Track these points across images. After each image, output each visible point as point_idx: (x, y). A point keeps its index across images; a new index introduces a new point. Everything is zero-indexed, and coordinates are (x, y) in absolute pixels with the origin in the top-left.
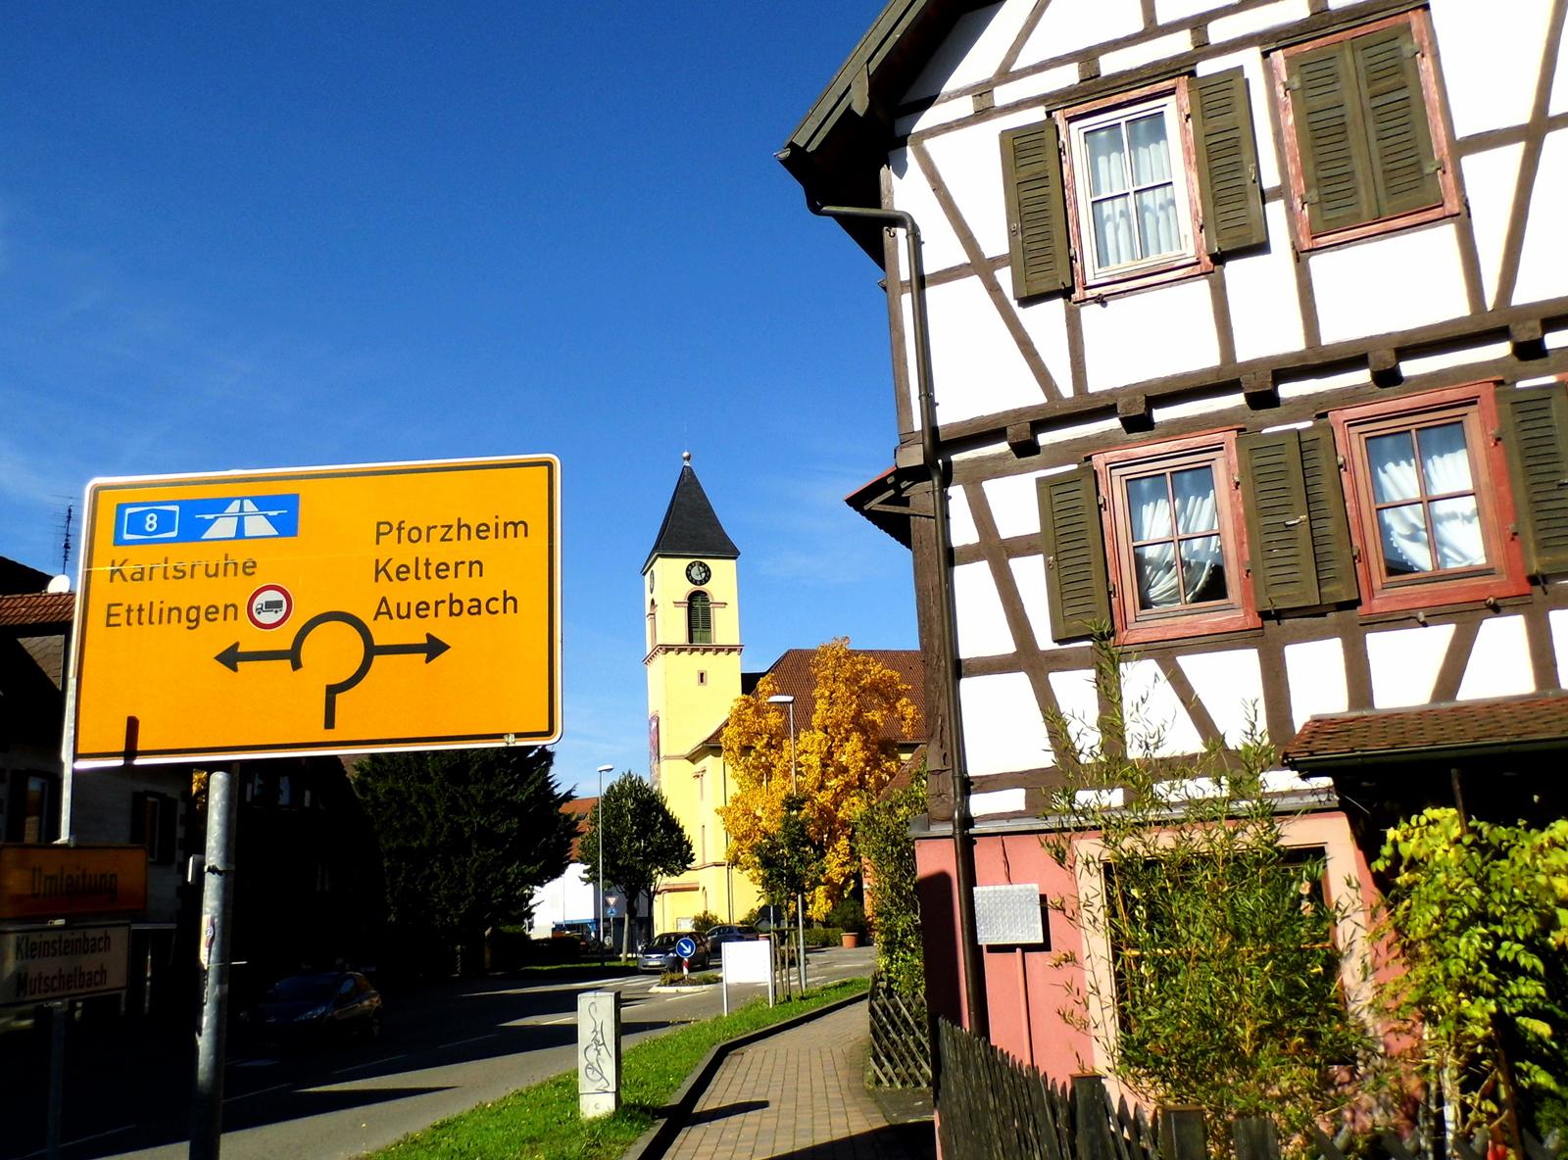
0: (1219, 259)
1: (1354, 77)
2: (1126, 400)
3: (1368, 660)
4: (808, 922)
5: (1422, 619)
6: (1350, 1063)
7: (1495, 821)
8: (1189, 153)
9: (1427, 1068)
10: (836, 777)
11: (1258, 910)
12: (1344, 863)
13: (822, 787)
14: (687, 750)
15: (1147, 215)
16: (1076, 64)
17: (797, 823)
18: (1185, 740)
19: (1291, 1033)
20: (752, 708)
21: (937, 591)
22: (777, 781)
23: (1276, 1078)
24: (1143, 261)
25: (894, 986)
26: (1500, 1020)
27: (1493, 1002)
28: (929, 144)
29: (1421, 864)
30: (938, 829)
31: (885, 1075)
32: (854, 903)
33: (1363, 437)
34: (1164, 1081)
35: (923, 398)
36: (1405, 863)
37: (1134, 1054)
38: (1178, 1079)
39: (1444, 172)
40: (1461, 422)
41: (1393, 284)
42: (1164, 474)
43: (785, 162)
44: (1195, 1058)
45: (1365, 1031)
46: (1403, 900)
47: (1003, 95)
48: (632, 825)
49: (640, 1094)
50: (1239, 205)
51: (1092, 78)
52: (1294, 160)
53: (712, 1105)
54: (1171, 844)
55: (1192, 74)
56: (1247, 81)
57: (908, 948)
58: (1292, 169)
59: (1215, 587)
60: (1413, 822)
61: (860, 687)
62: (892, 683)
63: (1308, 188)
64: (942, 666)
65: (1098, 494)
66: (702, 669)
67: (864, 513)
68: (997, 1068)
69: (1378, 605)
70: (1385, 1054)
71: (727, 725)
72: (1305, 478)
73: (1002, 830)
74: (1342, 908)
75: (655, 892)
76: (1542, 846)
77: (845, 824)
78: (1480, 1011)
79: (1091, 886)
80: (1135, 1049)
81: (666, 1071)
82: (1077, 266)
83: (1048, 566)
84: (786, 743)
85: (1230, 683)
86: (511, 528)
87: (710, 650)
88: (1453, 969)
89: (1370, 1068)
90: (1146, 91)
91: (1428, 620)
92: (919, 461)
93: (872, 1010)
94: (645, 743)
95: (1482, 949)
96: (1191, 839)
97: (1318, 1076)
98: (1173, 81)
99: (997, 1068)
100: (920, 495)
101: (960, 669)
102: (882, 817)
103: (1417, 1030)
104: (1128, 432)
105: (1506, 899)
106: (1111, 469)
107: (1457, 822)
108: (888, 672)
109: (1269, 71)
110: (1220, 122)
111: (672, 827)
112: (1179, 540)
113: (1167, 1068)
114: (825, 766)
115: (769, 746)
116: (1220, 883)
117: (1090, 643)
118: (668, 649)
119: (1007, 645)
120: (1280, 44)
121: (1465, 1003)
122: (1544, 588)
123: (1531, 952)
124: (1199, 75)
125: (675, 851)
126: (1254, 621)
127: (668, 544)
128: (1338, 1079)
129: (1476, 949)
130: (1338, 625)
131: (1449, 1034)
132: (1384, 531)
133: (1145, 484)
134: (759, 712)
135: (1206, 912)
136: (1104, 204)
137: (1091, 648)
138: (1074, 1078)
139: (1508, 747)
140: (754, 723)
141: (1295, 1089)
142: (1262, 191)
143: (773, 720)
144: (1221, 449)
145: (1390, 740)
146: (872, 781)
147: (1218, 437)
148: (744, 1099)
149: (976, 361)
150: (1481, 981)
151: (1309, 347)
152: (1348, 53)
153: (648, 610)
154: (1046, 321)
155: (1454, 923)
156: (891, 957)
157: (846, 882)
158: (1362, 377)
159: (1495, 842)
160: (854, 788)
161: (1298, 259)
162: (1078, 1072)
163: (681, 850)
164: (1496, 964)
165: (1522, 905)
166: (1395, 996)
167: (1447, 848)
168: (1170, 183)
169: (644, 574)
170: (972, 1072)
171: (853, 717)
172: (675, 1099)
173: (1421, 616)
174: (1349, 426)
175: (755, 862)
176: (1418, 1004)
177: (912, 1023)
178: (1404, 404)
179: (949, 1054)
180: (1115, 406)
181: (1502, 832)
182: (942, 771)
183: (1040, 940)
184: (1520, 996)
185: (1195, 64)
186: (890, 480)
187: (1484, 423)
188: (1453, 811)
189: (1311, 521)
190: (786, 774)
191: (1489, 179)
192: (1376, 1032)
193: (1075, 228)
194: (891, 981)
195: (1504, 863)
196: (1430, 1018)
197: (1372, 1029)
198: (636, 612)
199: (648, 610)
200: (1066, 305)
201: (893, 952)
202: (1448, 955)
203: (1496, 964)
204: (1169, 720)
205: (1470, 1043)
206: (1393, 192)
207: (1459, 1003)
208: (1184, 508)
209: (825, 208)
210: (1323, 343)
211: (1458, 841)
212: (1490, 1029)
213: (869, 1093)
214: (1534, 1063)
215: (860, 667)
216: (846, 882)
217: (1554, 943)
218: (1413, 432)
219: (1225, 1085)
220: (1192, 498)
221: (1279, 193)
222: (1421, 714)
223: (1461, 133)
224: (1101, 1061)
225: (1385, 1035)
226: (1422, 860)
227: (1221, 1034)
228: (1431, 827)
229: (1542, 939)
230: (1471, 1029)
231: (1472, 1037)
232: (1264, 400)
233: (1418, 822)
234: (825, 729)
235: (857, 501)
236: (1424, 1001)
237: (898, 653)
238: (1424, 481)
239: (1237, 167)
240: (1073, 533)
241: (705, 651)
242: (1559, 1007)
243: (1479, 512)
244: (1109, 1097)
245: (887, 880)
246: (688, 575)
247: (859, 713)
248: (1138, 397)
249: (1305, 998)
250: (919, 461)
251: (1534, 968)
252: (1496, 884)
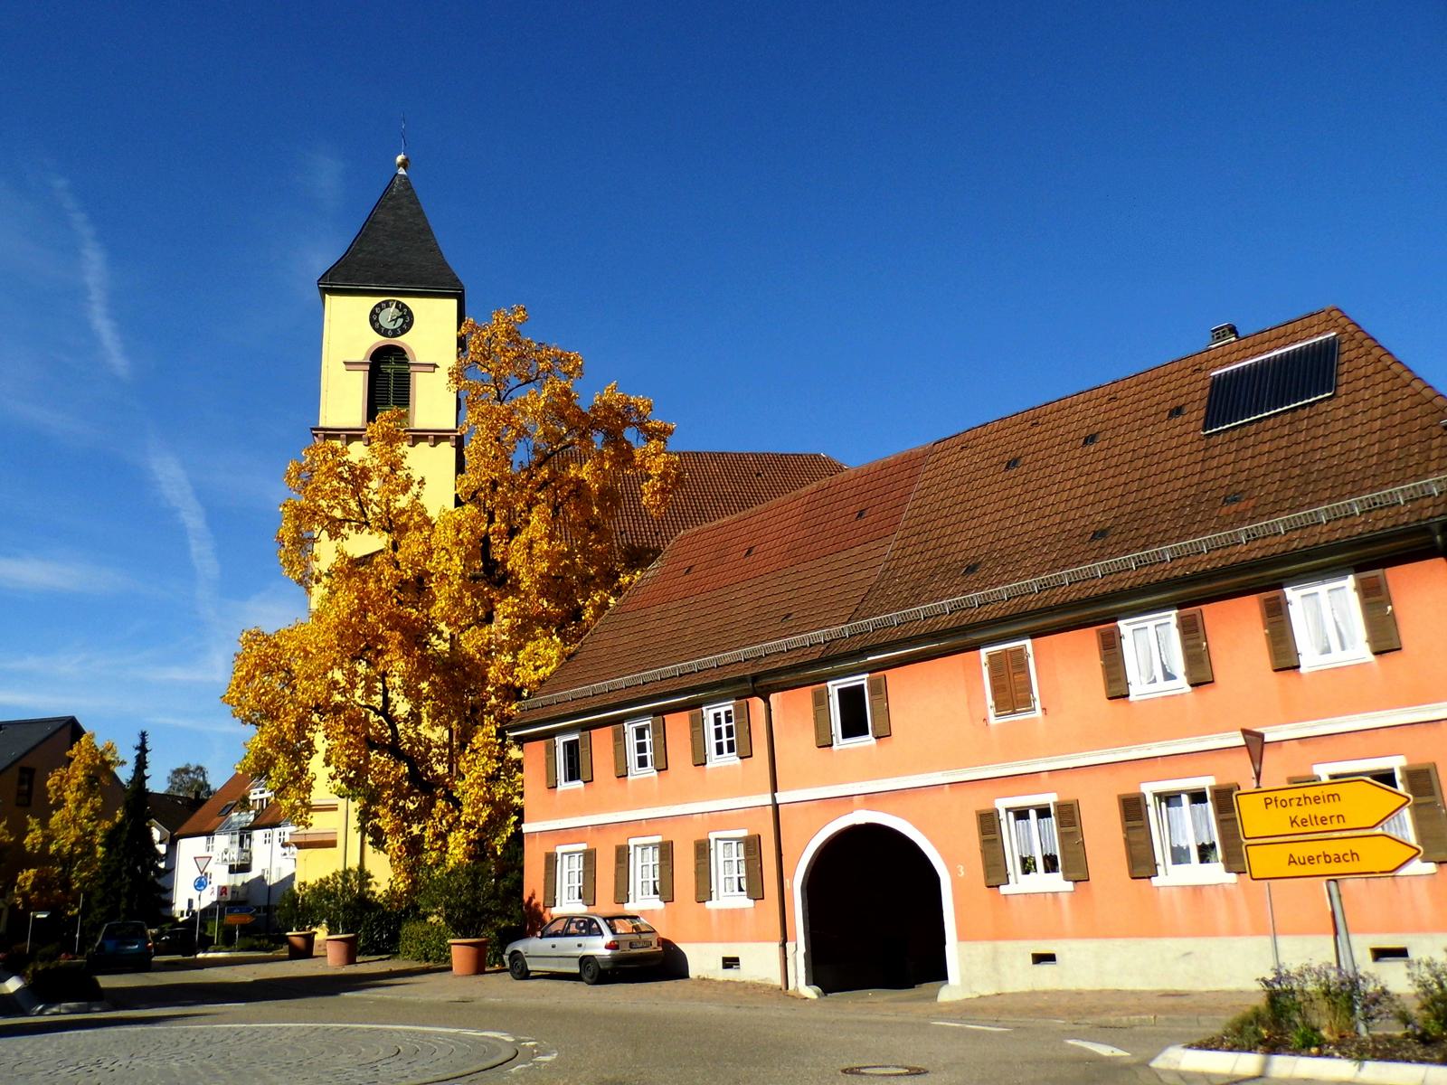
86: (1331, 797)
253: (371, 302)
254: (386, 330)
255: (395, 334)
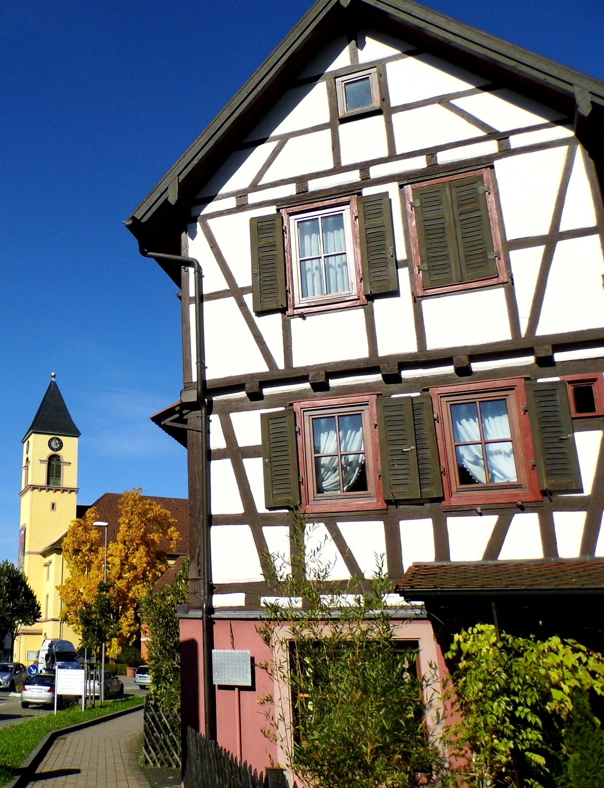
0: (371, 298)
1: (451, 204)
2: (314, 373)
3: (448, 533)
4: (107, 659)
5: (479, 511)
6: (427, 772)
7: (516, 635)
8: (356, 238)
9: (473, 779)
10: (129, 572)
11: (378, 677)
12: (429, 653)
13: (120, 577)
14: (41, 549)
15: (331, 270)
16: (294, 185)
17: (105, 600)
18: (340, 573)
19: (394, 752)
20: (82, 527)
21: (200, 474)
22: (94, 572)
23: (384, 778)
24: (328, 296)
25: (159, 704)
26: (516, 753)
27: (512, 742)
28: (210, 222)
29: (473, 656)
30: (192, 614)
31: (151, 758)
32: (134, 649)
33: (448, 403)
34: (320, 776)
35: (199, 364)
36: (464, 655)
37: (302, 758)
38: (327, 775)
39: (499, 259)
40: (505, 399)
41: (468, 319)
42: (334, 417)
43: (129, 227)
44: (339, 763)
45: (437, 754)
46: (462, 678)
47: (253, 198)
48: (6, 593)
49: (4, 759)
50: (382, 269)
51: (303, 192)
52: (415, 246)
53: (47, 769)
54: (329, 635)
55: (360, 194)
56: (390, 200)
57: (168, 680)
58: (414, 251)
59: (360, 484)
60: (470, 632)
61: (146, 519)
62: (166, 517)
63: (422, 262)
64: (199, 516)
65: (296, 425)
66: (54, 501)
67: (160, 426)
68: (222, 760)
69: (455, 501)
70: (449, 768)
71: (66, 535)
72: (414, 425)
73: (230, 617)
74: (427, 679)
75: (17, 634)
76: (544, 651)
77: (133, 601)
78: (504, 746)
79: (281, 655)
80: (304, 755)
81: (19, 746)
82: (290, 296)
83: (265, 465)
84: (100, 549)
85: (367, 540)
87: (59, 490)
88: (489, 720)
89: (439, 776)
90: (333, 202)
91: (482, 512)
92: (195, 399)
93: (145, 718)
94: (17, 541)
95: (506, 709)
96: (341, 633)
97: (409, 778)
98: (349, 197)
99: (222, 760)
100: (194, 418)
101: (211, 520)
102: (158, 601)
103: (467, 755)
104: (314, 392)
105: (521, 681)
106: (304, 411)
107: (495, 634)
108: (164, 511)
109: (403, 196)
110: (373, 222)
111: (30, 595)
112: (341, 455)
113: (322, 768)
114: (123, 564)
115: (90, 550)
116: (357, 661)
117: (287, 511)
118: (34, 488)
119: (238, 508)
120: (410, 181)
121: (496, 741)
122: (550, 498)
123: (535, 714)
124: (364, 195)
125: (30, 610)
126: (382, 505)
127: (39, 426)
128: (421, 781)
129: (503, 710)
130: (430, 510)
131: (486, 759)
132: (459, 458)
133: (323, 421)
134: (86, 529)
135: (348, 676)
136: (307, 262)
137: (288, 513)
138: (267, 770)
139: (525, 592)
140: (82, 536)
141: (395, 785)
142: (396, 261)
143: (94, 535)
144: (367, 404)
145: (458, 582)
146: (150, 575)
147: (366, 398)
148: (66, 767)
149: (229, 346)
150: (505, 729)
151: (419, 351)
152: (447, 189)
153: (24, 464)
154: (270, 325)
155: (490, 693)
156: (157, 686)
157: (131, 636)
158: (449, 369)
159: (516, 647)
160: (139, 579)
161: (415, 301)
162: (270, 766)
163: (33, 610)
164: (514, 720)
165: (530, 686)
166: (456, 734)
167: (489, 648)
168: (345, 253)
169: (24, 442)
170: (206, 761)
171: (141, 536)
172: (26, 764)
173: (479, 509)
174: (441, 397)
175: (77, 621)
176: (469, 739)
177: (169, 727)
178: (473, 386)
179: (192, 749)
180: (308, 376)
181: (521, 641)
182: (197, 579)
183: (250, 684)
184: (528, 739)
185: (362, 189)
186: (177, 409)
187: (518, 402)
188: (492, 627)
189: (417, 449)
190: (99, 568)
191: (524, 265)
192: (444, 755)
193: (290, 275)
194: (157, 700)
195: (520, 659)
196: (475, 749)
197: (442, 753)
198: (17, 465)
199: (24, 464)
200: (283, 317)
201: (159, 683)
202: (487, 712)
203: (514, 720)
204: (333, 563)
205: (498, 765)
206: (470, 267)
207: (492, 740)
208: (345, 437)
209: (149, 253)
210: (428, 349)
211: (494, 644)
212: (510, 758)
213: (142, 769)
214: (536, 780)
215: (147, 507)
216: (131, 636)
217: (549, 709)
218: (478, 403)
219: (354, 780)
220: (349, 431)
221: (405, 263)
222: (476, 566)
223: (510, 237)
224: (283, 760)
225: (449, 757)
226: (474, 654)
227: (354, 750)
228: (480, 635)
229: (542, 706)
230: (499, 757)
231: (499, 762)
232: (393, 379)
233: (472, 631)
234: (124, 543)
235: (157, 419)
236: (473, 739)
237: (170, 500)
238: (483, 431)
239: (383, 247)
240: (281, 446)
241: (56, 490)
242: (550, 748)
243: (514, 451)
244: (287, 782)
245: (158, 638)
246: (50, 445)
247: (145, 534)
248: (321, 372)
249: (403, 732)
250: (195, 399)
251: (536, 723)
252: (516, 672)
253: (48, 437)
254: (56, 449)
255: (57, 450)
